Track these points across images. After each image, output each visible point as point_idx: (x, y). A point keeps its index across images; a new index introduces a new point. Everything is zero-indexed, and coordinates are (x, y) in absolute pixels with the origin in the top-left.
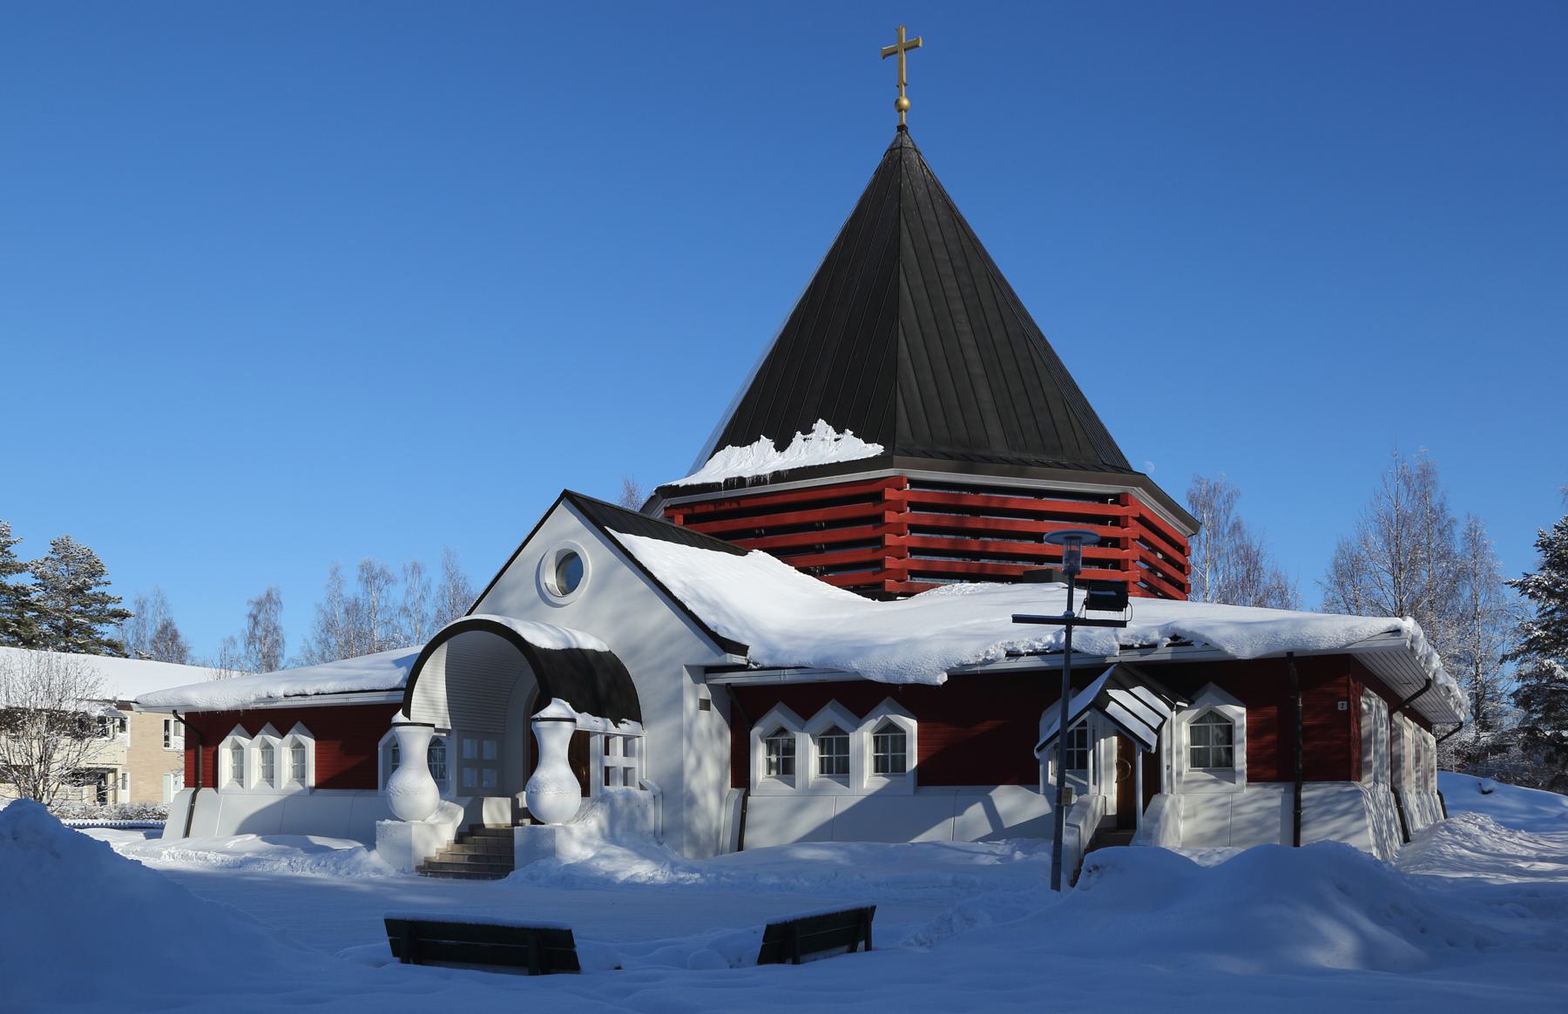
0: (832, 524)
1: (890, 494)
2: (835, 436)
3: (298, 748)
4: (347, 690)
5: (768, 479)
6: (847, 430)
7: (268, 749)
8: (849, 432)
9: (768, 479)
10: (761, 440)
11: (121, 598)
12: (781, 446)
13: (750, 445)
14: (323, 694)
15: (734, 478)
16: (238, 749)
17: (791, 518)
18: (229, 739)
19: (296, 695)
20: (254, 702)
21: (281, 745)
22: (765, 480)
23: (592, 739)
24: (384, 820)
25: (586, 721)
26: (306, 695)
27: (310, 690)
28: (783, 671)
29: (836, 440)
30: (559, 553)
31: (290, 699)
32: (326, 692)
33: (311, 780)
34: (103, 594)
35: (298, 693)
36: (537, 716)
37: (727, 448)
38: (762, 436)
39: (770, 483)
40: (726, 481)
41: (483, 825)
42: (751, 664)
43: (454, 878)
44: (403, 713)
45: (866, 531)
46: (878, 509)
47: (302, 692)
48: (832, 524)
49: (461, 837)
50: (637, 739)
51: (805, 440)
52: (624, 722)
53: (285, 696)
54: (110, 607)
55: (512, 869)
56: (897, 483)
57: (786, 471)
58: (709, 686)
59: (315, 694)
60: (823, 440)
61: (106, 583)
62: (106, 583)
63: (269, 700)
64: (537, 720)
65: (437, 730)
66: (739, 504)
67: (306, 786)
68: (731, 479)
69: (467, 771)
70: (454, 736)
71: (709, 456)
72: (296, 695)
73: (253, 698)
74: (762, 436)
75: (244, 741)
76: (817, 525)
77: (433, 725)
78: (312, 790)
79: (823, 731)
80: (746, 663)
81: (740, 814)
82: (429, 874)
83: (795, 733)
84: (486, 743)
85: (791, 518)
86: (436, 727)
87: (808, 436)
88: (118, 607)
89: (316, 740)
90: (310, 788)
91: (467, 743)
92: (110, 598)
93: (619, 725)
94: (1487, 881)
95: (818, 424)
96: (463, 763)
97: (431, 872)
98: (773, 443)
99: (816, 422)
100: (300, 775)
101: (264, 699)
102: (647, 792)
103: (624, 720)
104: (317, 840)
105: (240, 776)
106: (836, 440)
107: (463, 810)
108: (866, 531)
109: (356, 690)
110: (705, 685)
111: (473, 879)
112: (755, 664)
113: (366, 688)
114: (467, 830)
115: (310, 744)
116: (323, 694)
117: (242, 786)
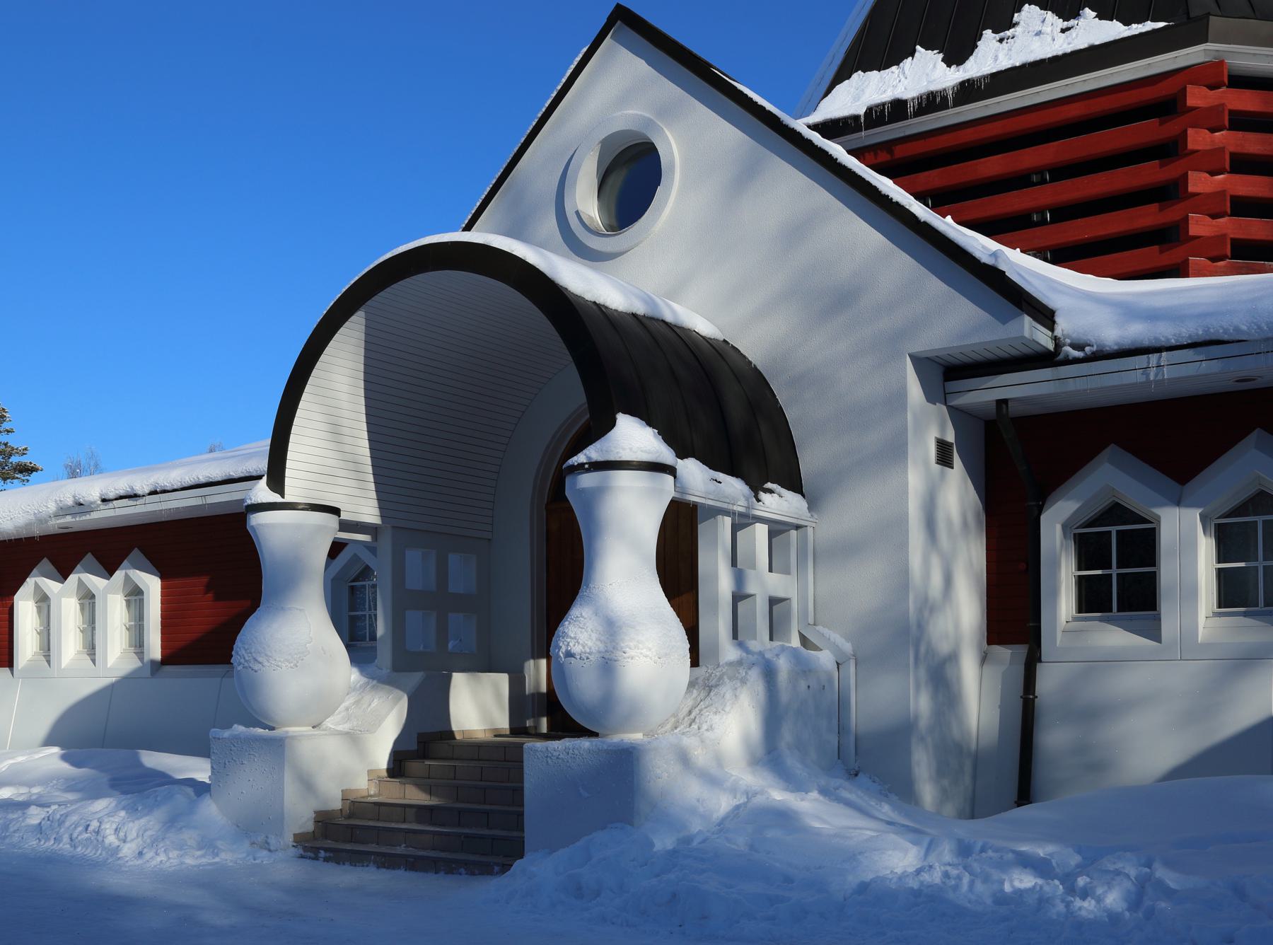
0: (1062, 172)
1: (1197, 97)
2: (1061, 24)
3: (135, 595)
4: (203, 480)
5: (950, 97)
6: (1087, 10)
7: (88, 598)
8: (1089, 13)
9: (950, 97)
10: (917, 54)
11: (26, 449)
12: (955, 57)
13: (898, 64)
14: (164, 491)
15: (883, 104)
16: (43, 600)
17: (992, 166)
18: (30, 582)
19: (121, 497)
20: (56, 516)
21: (107, 590)
22: (944, 98)
23: (702, 528)
24: (229, 726)
25: (694, 473)
26: (134, 496)
27: (141, 484)
28: (1153, 358)
29: (1063, 31)
30: (606, 143)
31: (111, 505)
32: (169, 487)
33: (155, 650)
34: (6, 444)
35: (122, 493)
36: (581, 458)
37: (855, 76)
38: (918, 47)
39: (955, 105)
40: (869, 111)
41: (450, 734)
42: (1068, 349)
43: (380, 866)
44: (268, 484)
45: (1148, 173)
46: (1169, 129)
47: (128, 490)
48: (1062, 172)
49: (399, 764)
50: (793, 533)
51: (1001, 41)
52: (771, 491)
53: (104, 500)
54: (15, 459)
55: (517, 851)
56: (1211, 75)
57: (985, 77)
58: (951, 409)
59: (152, 493)
60: (1039, 33)
61: (8, 432)
62: (8, 432)
63: (78, 509)
64: (580, 468)
65: (346, 526)
66: (891, 152)
67: (146, 659)
68: (877, 106)
69: (414, 618)
70: (386, 545)
71: (822, 96)
72: (121, 497)
73: (52, 507)
74: (918, 47)
75: (52, 586)
76: (1035, 178)
77: (335, 511)
78: (156, 667)
79: (1226, 509)
80: (1051, 346)
81: (1019, 704)
82: (322, 854)
83: (1158, 511)
84: (453, 559)
85: (992, 166)
86: (344, 516)
87: (1009, 33)
88: (24, 460)
89: (162, 578)
90: (153, 662)
91: (414, 557)
92: (13, 449)
93: (762, 495)
94: (532, 684)
95: (1023, 13)
96: (403, 602)
97: (326, 850)
98: (941, 56)
99: (1019, 11)
100: (138, 643)
101: (69, 508)
102: (724, 662)
103: (769, 485)
104: (154, 760)
105: (46, 648)
106: (1063, 31)
107: (405, 699)
108: (1148, 173)
109: (220, 479)
110: (944, 408)
111: (425, 870)
112: (1076, 346)
113: (235, 475)
114: (413, 746)
115: (152, 585)
116: (164, 491)
117: (94, 661)
